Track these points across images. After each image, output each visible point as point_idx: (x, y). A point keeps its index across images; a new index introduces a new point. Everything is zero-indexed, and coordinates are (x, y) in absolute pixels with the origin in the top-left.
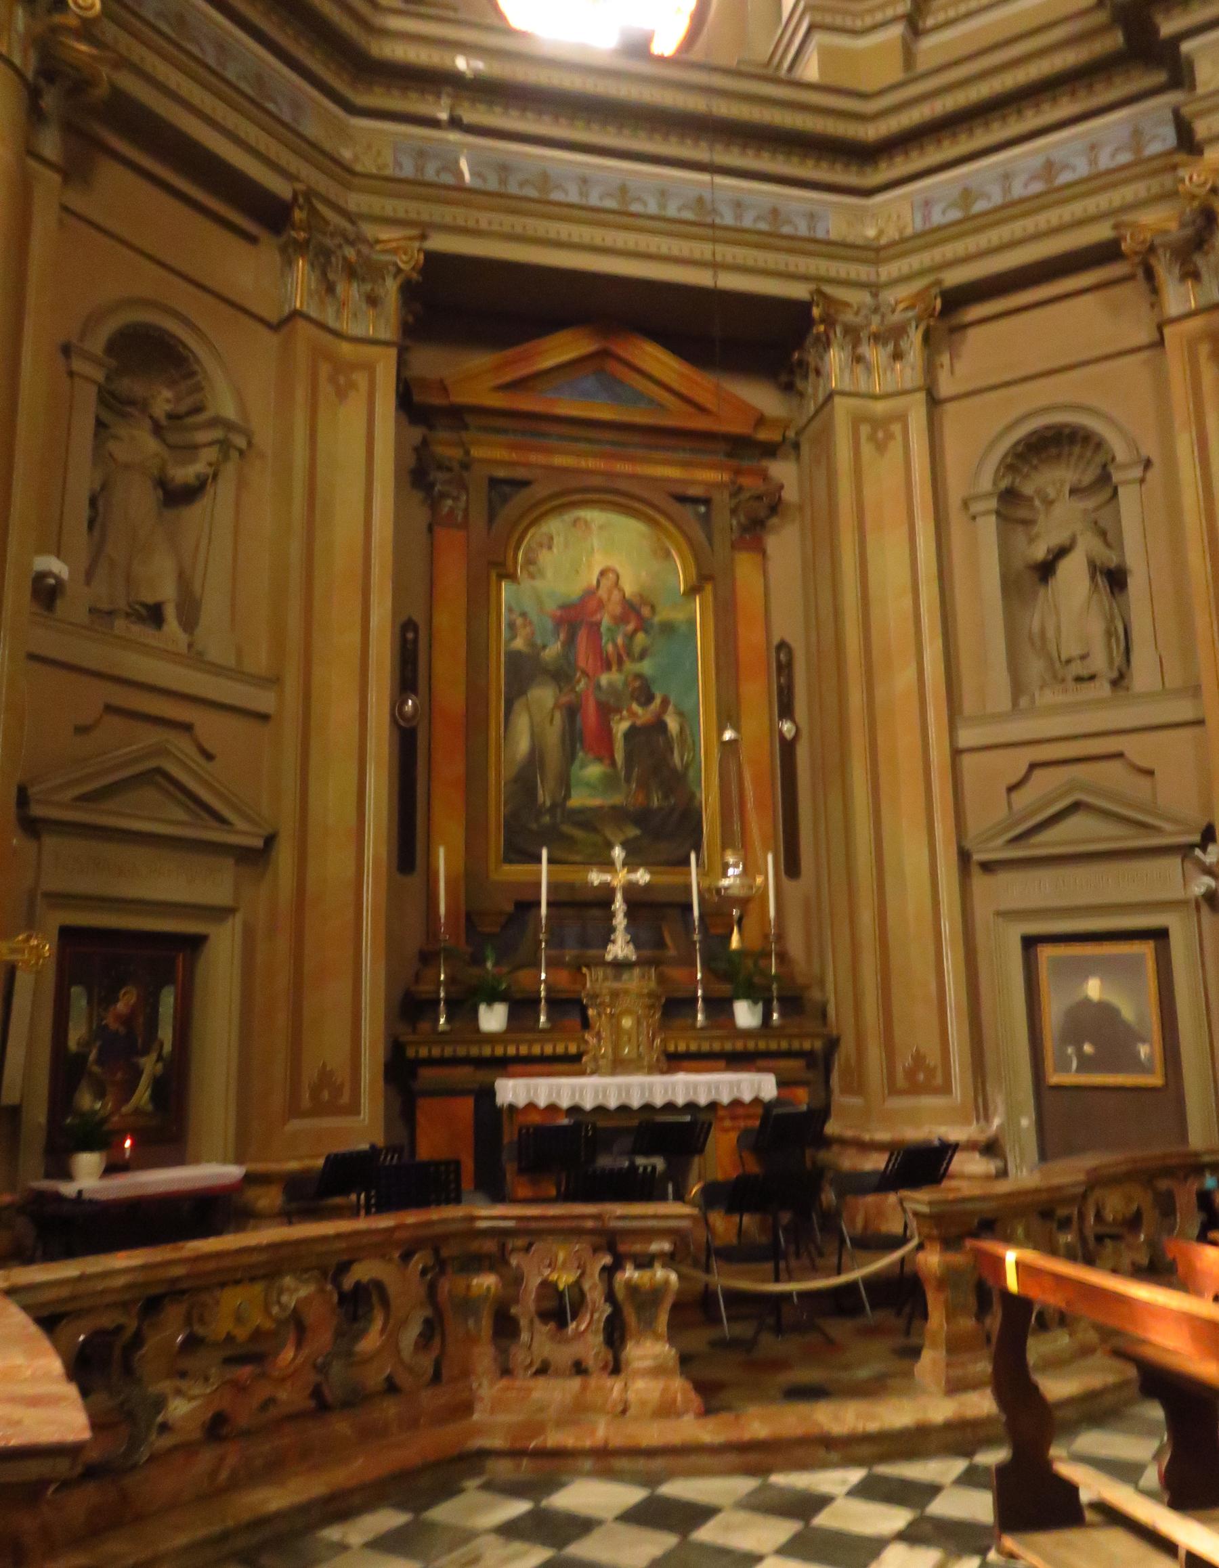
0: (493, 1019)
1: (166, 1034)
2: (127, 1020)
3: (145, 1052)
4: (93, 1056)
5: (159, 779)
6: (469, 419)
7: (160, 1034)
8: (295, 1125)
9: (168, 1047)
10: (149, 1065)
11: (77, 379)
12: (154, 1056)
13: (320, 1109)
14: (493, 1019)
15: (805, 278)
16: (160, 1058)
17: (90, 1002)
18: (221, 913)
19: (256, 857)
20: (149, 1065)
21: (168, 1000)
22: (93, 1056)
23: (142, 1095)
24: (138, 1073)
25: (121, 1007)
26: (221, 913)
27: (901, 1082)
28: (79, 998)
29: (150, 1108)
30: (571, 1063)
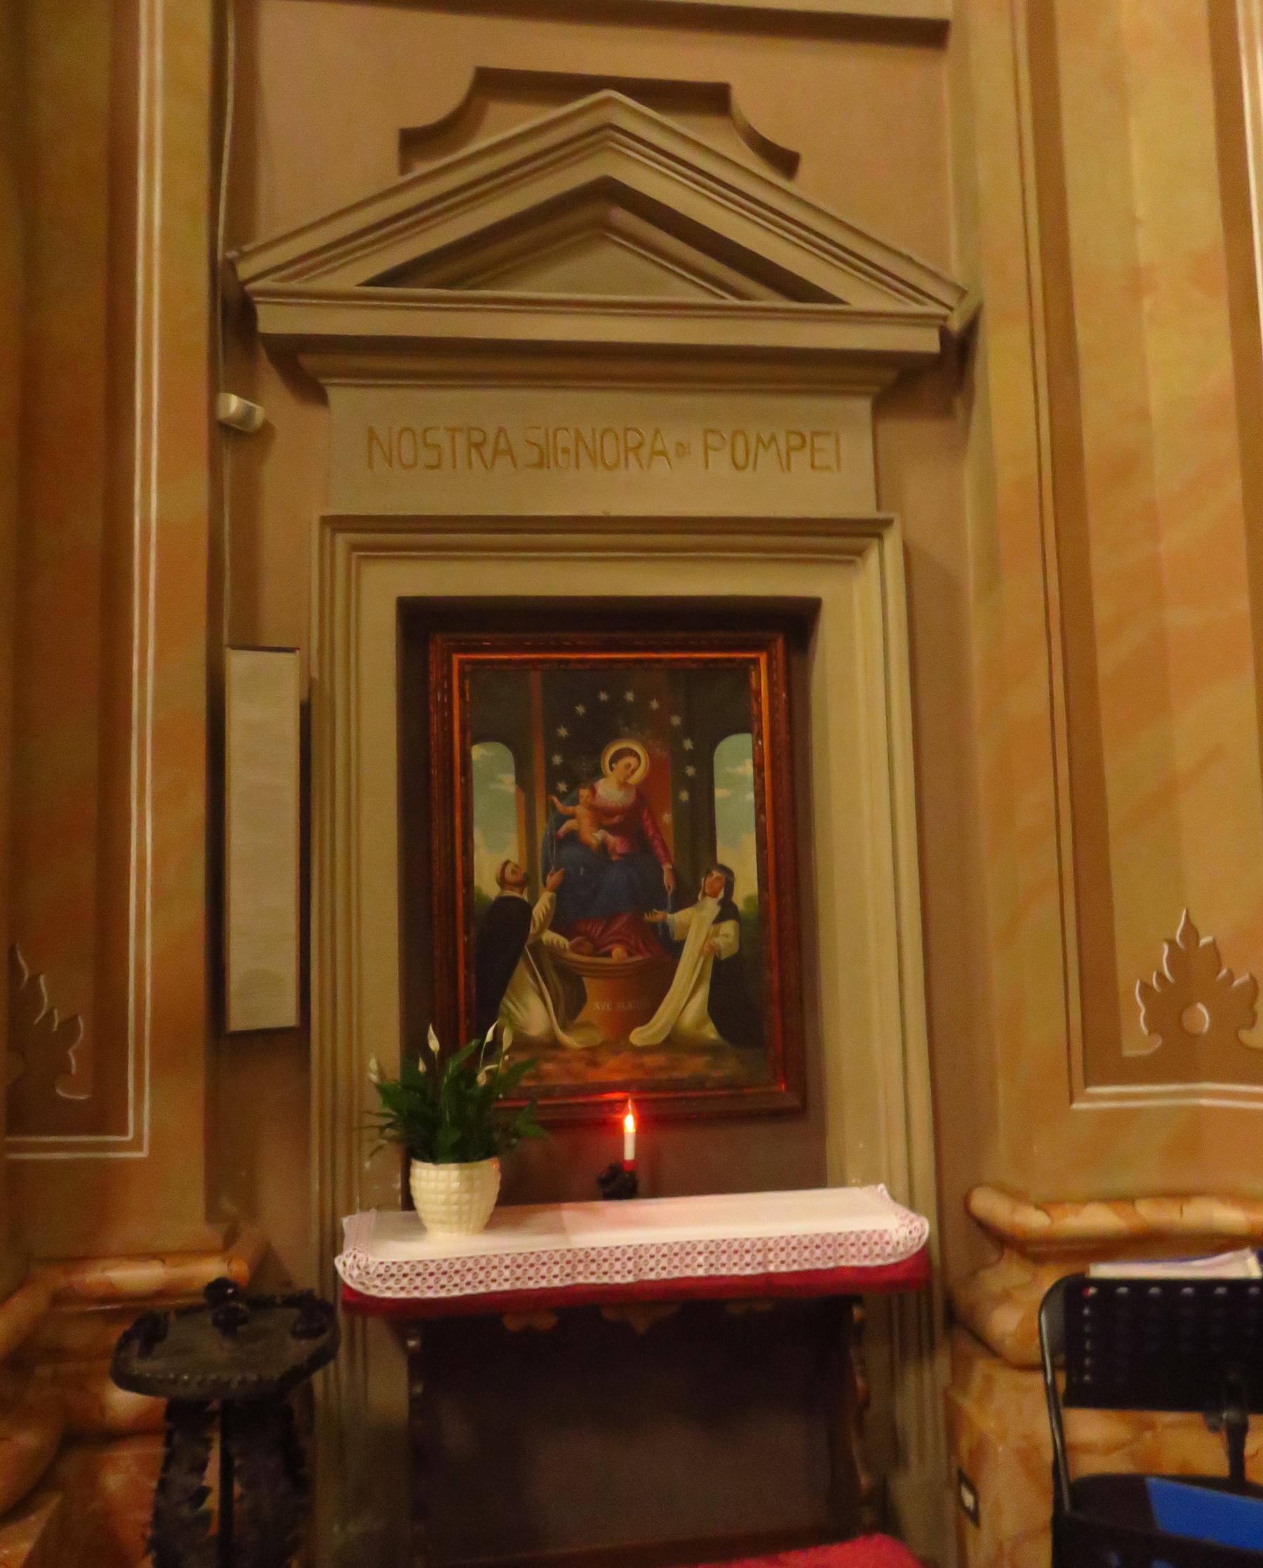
1: (739, 851)
2: (631, 822)
3: (686, 897)
4: (542, 907)
5: (621, 216)
7: (724, 855)
8: (1104, 1097)
9: (747, 887)
10: (700, 930)
12: (710, 907)
13: (1178, 1059)
16: (727, 911)
17: (523, 781)
18: (843, 539)
19: (930, 381)
20: (700, 930)
21: (736, 765)
22: (542, 907)
23: (686, 1004)
24: (669, 948)
25: (609, 791)
26: (843, 539)
28: (493, 772)
29: (710, 1033)
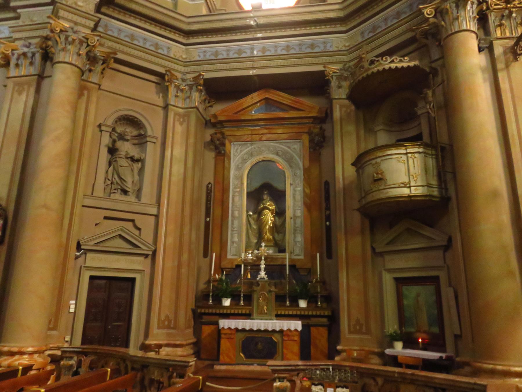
0: (227, 302)
6: (226, 124)
11: (103, 132)
14: (227, 302)
15: (340, 62)
27: (352, 329)
30: (248, 316)
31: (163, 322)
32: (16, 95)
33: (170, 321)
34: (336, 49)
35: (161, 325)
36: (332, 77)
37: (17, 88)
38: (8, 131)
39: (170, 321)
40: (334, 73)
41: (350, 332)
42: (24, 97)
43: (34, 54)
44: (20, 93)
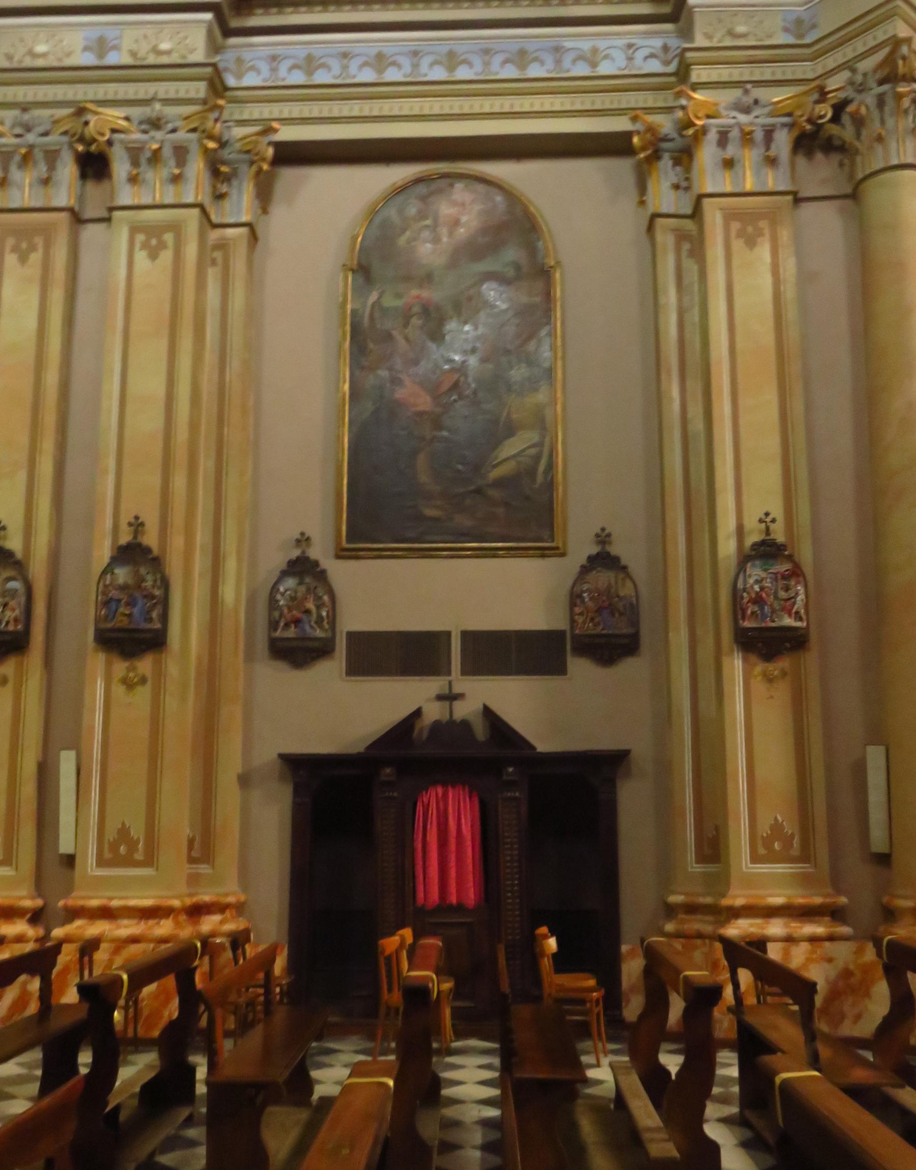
27: (107, 855)
31: (768, 842)
32: (738, 245)
33: (132, 845)
34: (127, 60)
35: (107, 855)
36: (110, 143)
37: (735, 226)
38: (739, 345)
39: (787, 842)
40: (114, 131)
41: (755, 859)
42: (764, 251)
43: (769, 134)
44: (751, 243)
